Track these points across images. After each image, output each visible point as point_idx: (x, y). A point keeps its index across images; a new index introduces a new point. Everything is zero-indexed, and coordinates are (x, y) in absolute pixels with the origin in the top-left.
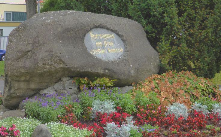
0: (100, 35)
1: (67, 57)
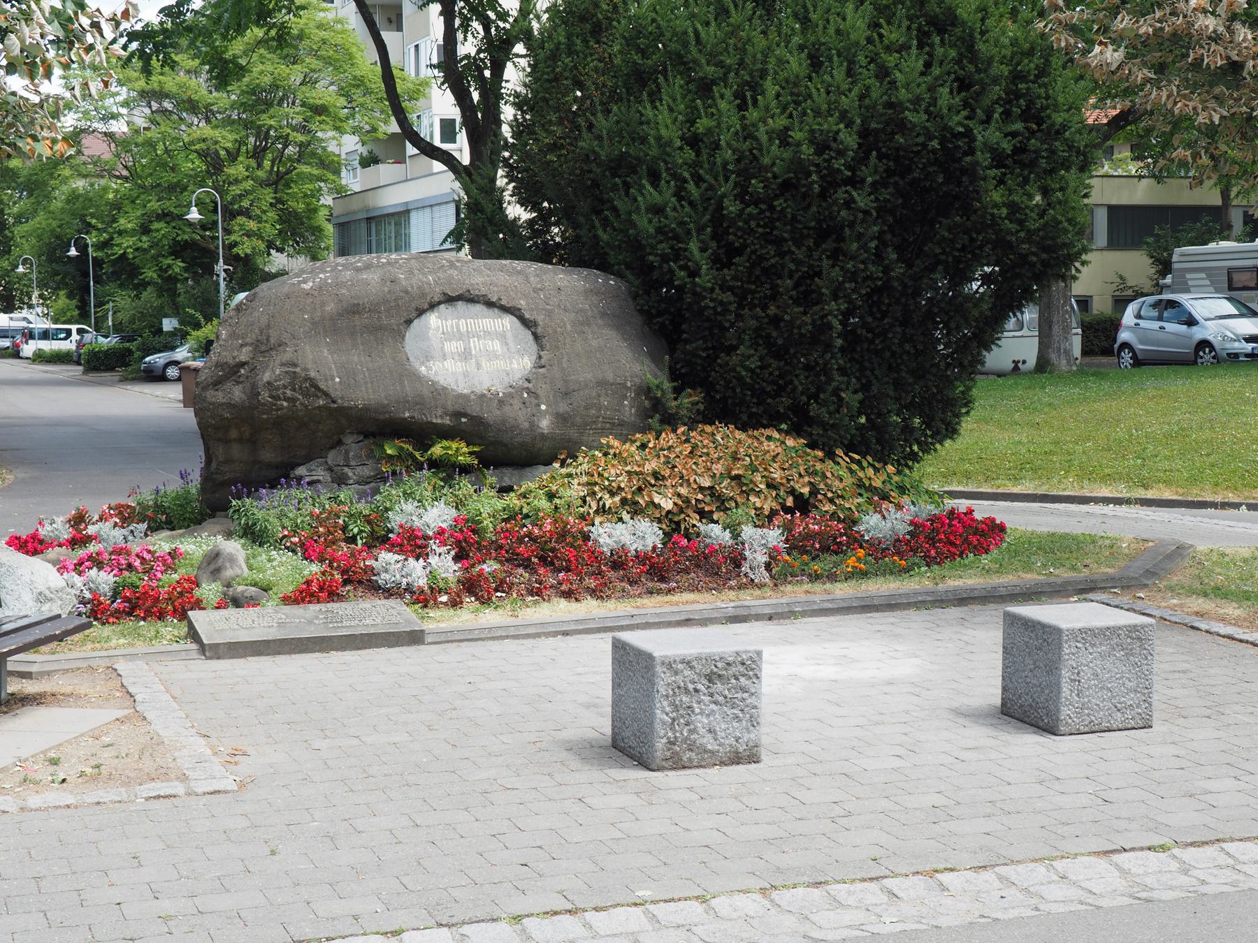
1: (337, 380)
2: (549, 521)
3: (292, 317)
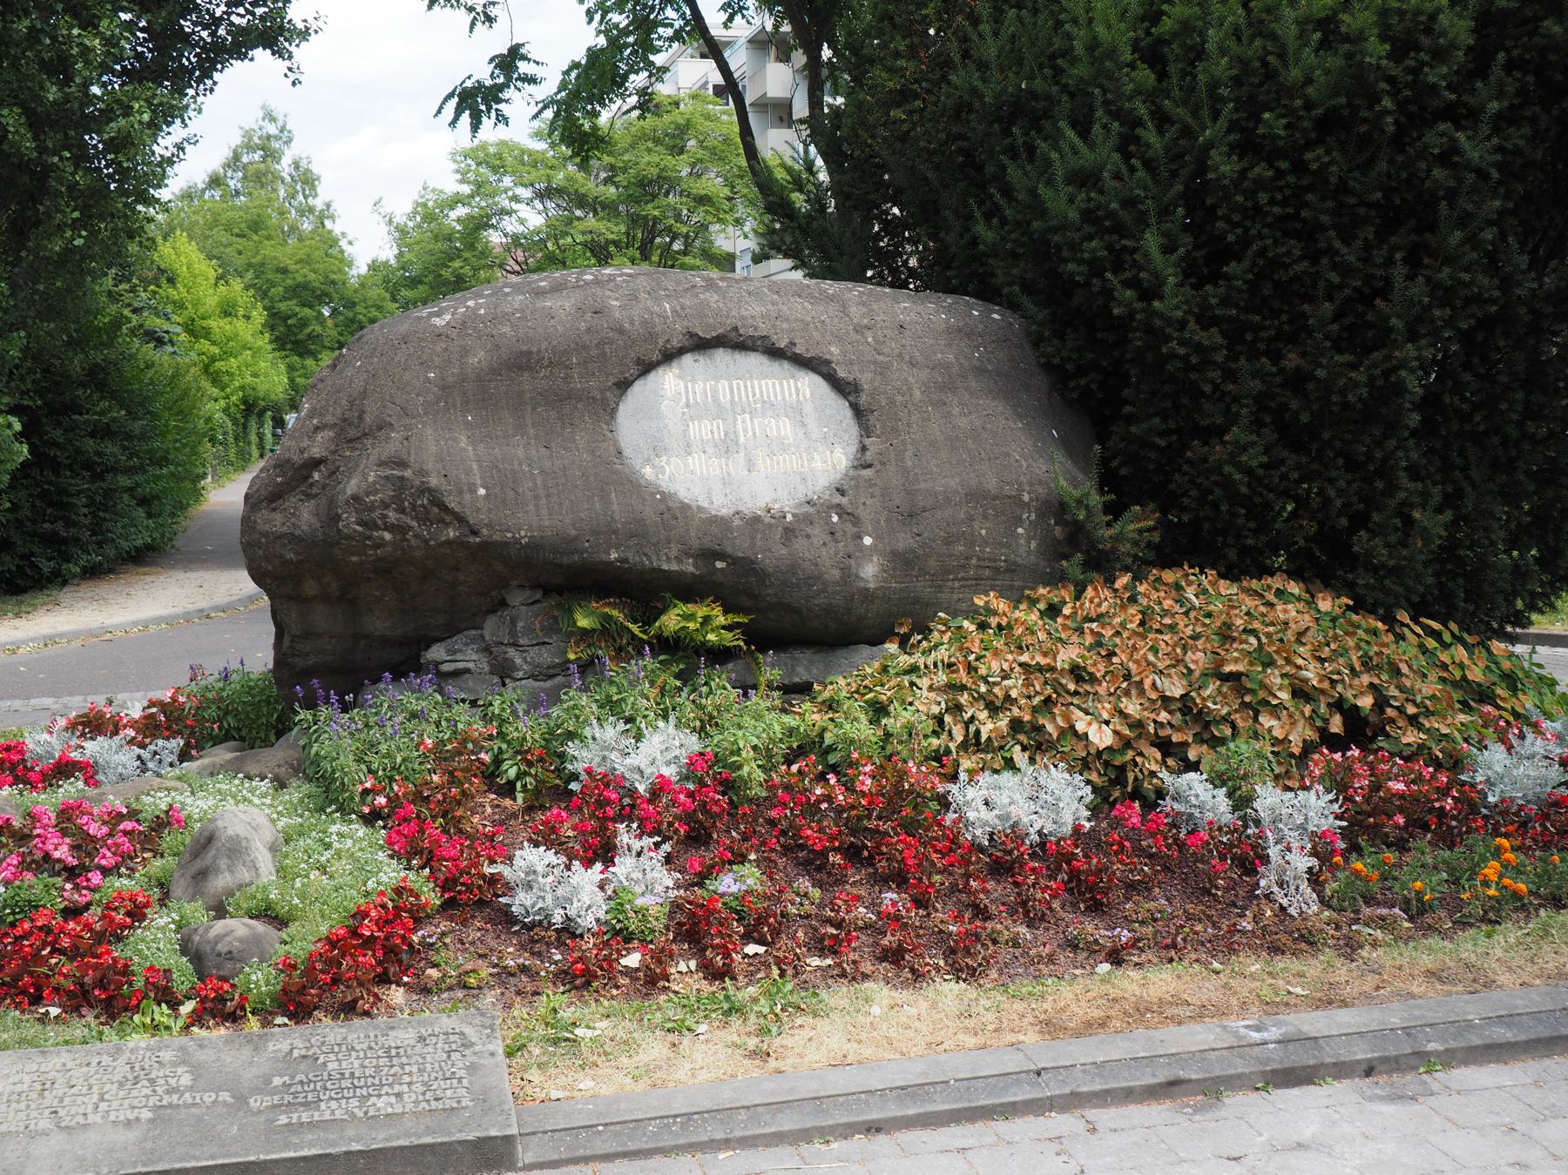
0: (723, 385)
1: (482, 492)
2: (868, 769)
3: (407, 376)
